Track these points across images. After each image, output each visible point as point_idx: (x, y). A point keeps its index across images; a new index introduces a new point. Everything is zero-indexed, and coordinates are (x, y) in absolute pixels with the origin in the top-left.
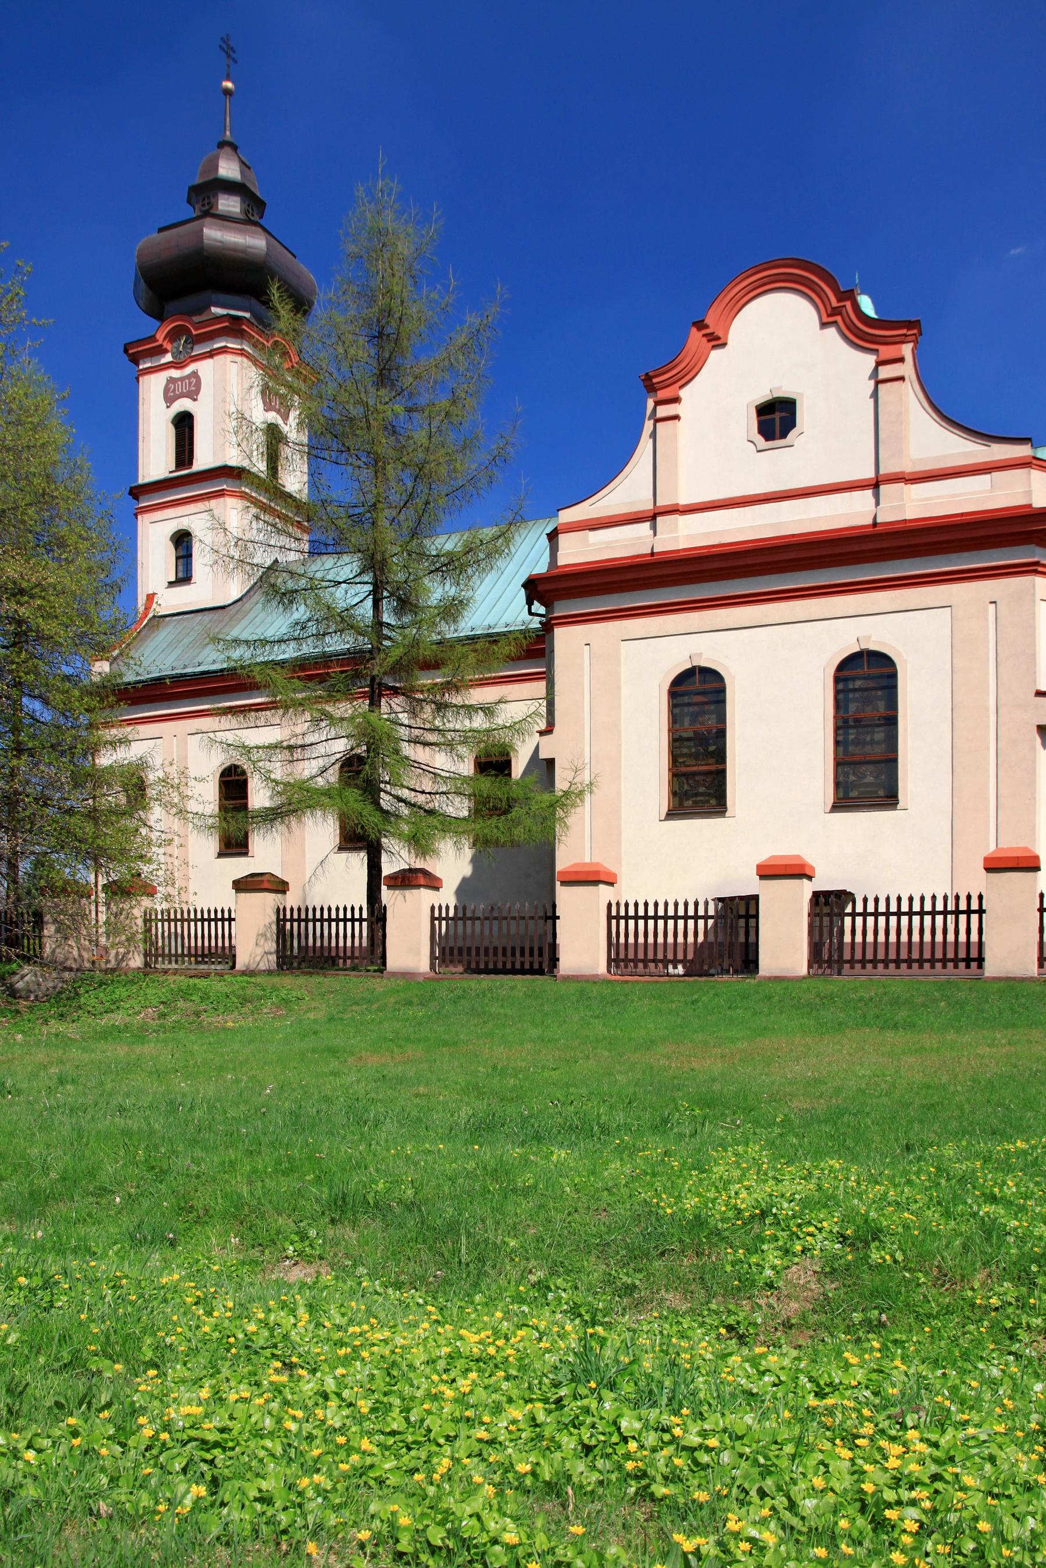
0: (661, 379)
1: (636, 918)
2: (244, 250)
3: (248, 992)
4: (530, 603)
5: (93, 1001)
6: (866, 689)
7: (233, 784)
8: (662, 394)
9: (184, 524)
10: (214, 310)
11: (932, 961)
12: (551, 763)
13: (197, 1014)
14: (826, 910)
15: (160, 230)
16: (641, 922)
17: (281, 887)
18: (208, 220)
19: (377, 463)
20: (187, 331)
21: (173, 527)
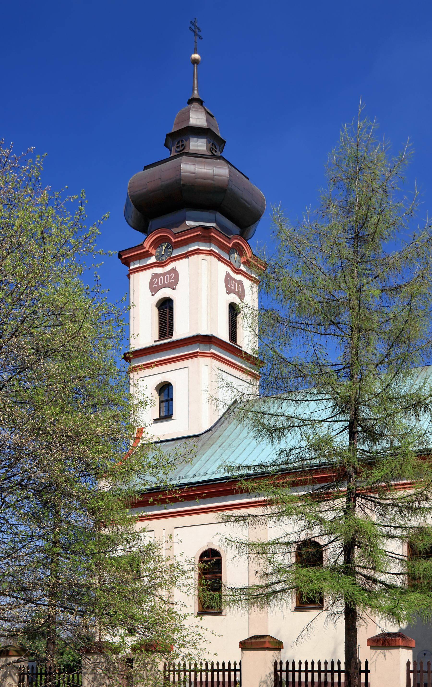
2: (212, 177)
10: (188, 223)
15: (146, 168)
17: (278, 646)
18: (184, 158)
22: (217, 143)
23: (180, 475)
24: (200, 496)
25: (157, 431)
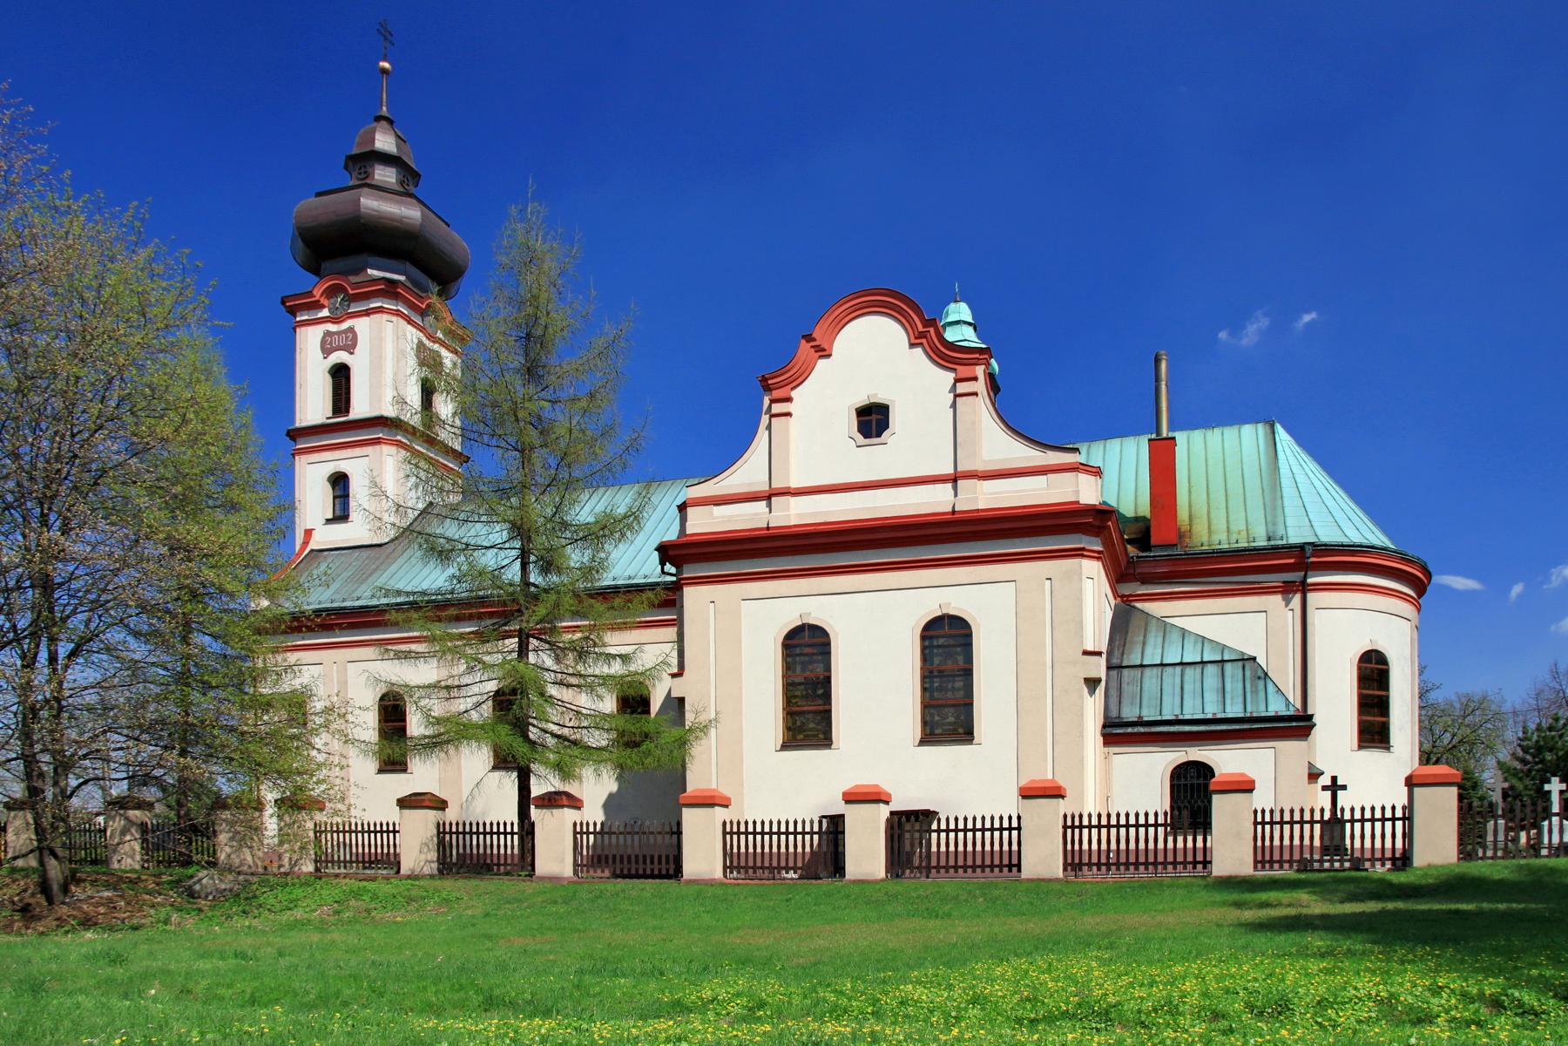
0: (777, 381)
1: (498, 833)
2: (401, 220)
3: (414, 893)
4: (662, 563)
5: (272, 901)
6: (947, 647)
7: (392, 711)
8: (776, 394)
9: (344, 467)
11: (983, 867)
12: (681, 700)
13: (368, 911)
14: (917, 826)
15: (319, 194)
16: (783, 837)
17: (441, 805)
18: (366, 190)
19: (524, 451)
20: (344, 290)
21: (331, 468)
22: (409, 175)
23: (355, 595)
24: (340, 626)
25: (328, 536)
